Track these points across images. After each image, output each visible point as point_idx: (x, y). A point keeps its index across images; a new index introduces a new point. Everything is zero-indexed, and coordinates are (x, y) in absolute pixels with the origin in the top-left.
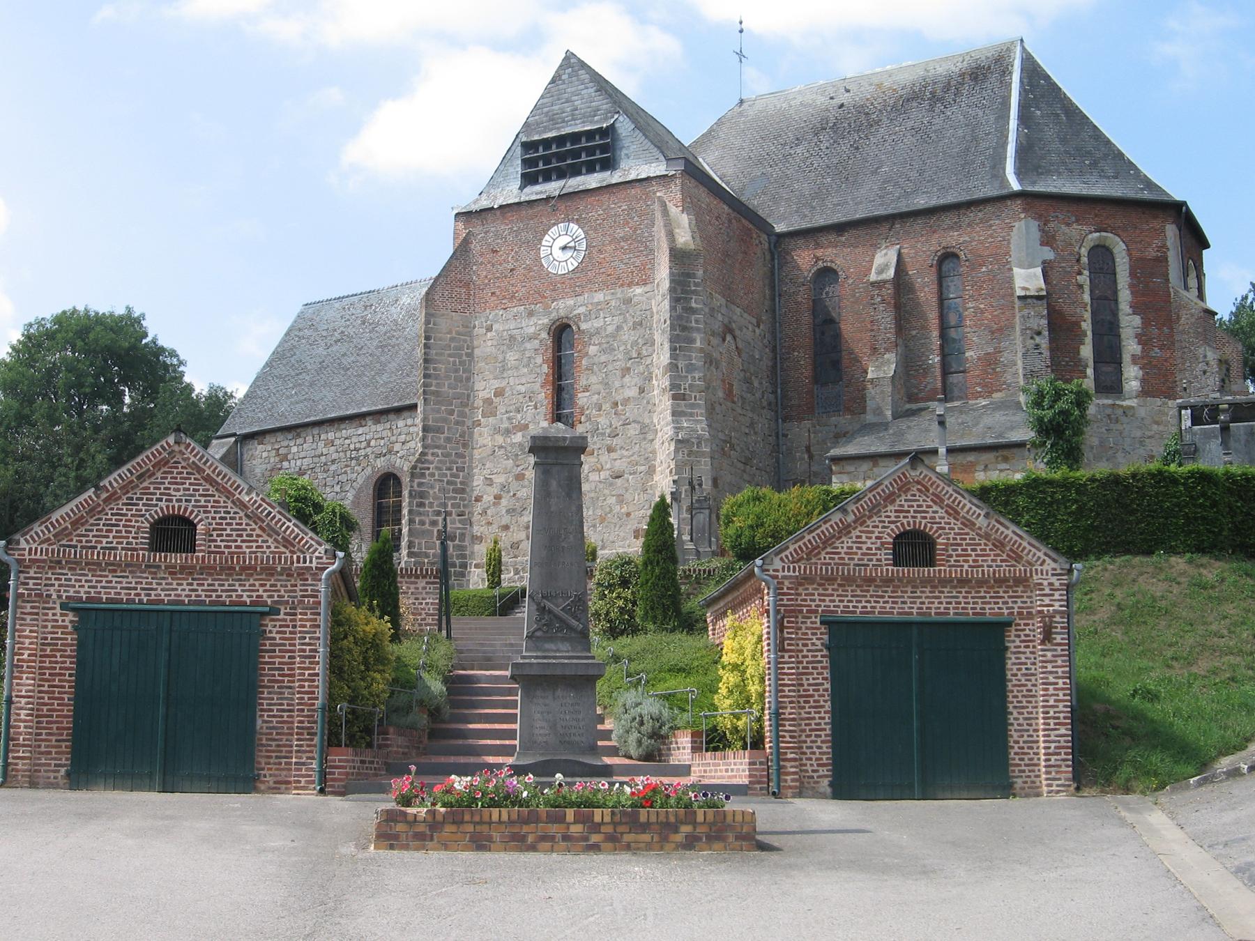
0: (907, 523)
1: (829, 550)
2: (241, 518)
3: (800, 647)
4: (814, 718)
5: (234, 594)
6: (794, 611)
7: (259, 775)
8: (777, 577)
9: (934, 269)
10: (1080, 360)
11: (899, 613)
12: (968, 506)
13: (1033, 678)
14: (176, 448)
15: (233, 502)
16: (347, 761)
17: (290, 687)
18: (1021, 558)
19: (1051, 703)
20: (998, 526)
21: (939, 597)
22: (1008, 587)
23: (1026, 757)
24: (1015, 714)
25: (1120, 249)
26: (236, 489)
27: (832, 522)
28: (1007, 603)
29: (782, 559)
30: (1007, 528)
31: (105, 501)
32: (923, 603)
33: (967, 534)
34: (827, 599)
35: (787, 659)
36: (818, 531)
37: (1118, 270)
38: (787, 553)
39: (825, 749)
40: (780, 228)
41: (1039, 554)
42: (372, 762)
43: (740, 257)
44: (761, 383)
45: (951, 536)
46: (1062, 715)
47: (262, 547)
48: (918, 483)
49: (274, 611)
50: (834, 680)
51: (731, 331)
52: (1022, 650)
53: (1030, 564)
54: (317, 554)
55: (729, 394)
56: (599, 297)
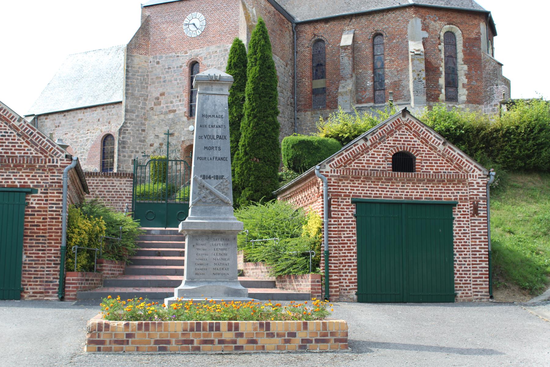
0: (400, 147)
1: (356, 161)
2: (14, 136)
3: (340, 216)
4: (347, 256)
5: (10, 181)
6: (337, 195)
7: (24, 288)
8: (327, 176)
9: (370, 41)
10: (439, 85)
11: (395, 198)
12: (433, 137)
13: (467, 235)
15: (10, 126)
16: (78, 280)
17: (43, 236)
18: (462, 168)
20: (449, 150)
21: (417, 189)
22: (454, 184)
23: (463, 279)
24: (458, 255)
25: (458, 33)
26: (11, 119)
27: (359, 146)
28: (453, 193)
29: (330, 166)
30: (455, 151)
32: (408, 192)
33: (433, 154)
34: (355, 189)
35: (332, 222)
36: (351, 150)
37: (457, 43)
38: (333, 162)
39: (353, 274)
40: (298, 20)
41: (471, 166)
42: (92, 280)
43: (279, 32)
44: (287, 93)
45: (424, 155)
46: (483, 256)
47: (27, 153)
48: (406, 125)
49: (32, 191)
50: (359, 234)
52: (462, 219)
53: (467, 172)
54: (60, 158)
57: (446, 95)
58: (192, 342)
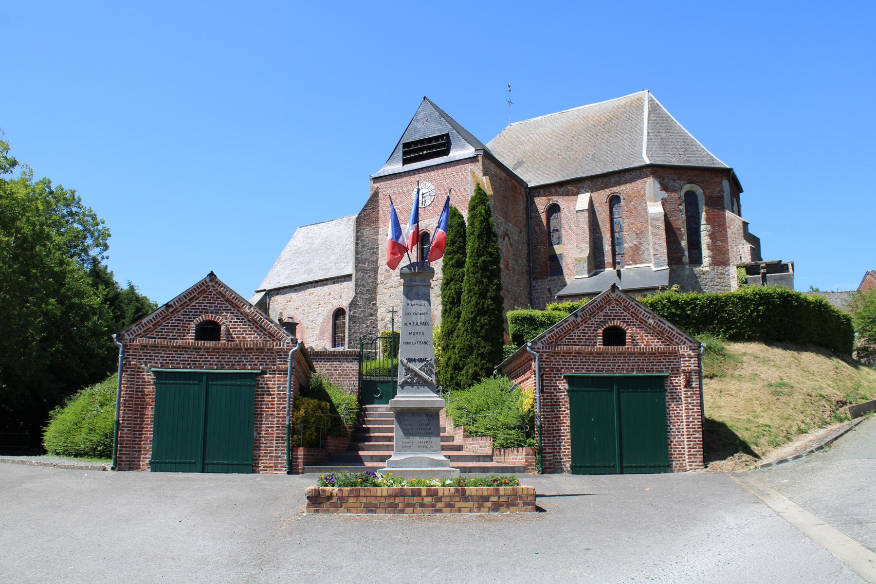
14: (210, 284)
19: (691, 420)
25: (699, 191)
31: (171, 313)
43: (511, 198)
48: (616, 300)
51: (508, 235)
57: (689, 257)
58: (397, 505)
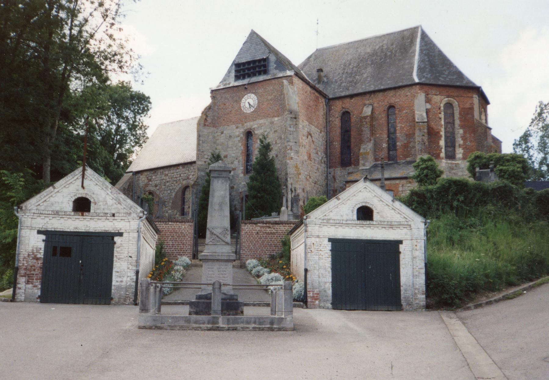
51: (310, 135)
55: (309, 157)
56: (262, 121)
57: (446, 153)
